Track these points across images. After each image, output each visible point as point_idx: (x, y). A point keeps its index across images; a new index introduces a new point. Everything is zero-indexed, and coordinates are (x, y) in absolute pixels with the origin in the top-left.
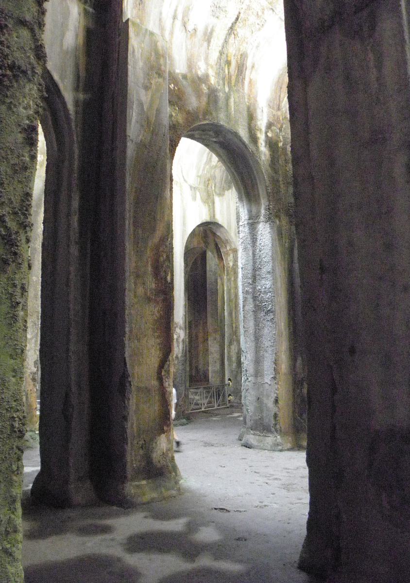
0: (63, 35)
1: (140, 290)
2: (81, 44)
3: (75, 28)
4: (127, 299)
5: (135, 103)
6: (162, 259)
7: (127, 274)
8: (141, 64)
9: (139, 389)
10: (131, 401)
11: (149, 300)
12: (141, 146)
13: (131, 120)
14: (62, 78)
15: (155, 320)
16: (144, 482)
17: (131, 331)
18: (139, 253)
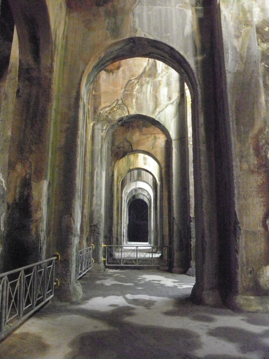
0: (183, 29)
1: (245, 166)
2: (196, 30)
3: (191, 22)
4: (235, 172)
5: (229, 49)
6: (261, 144)
7: (234, 156)
8: (231, 24)
9: (247, 232)
10: (240, 241)
11: (253, 172)
12: (237, 74)
13: (228, 61)
14: (186, 52)
15: (258, 185)
16: (252, 297)
17: (239, 194)
18: (242, 142)
